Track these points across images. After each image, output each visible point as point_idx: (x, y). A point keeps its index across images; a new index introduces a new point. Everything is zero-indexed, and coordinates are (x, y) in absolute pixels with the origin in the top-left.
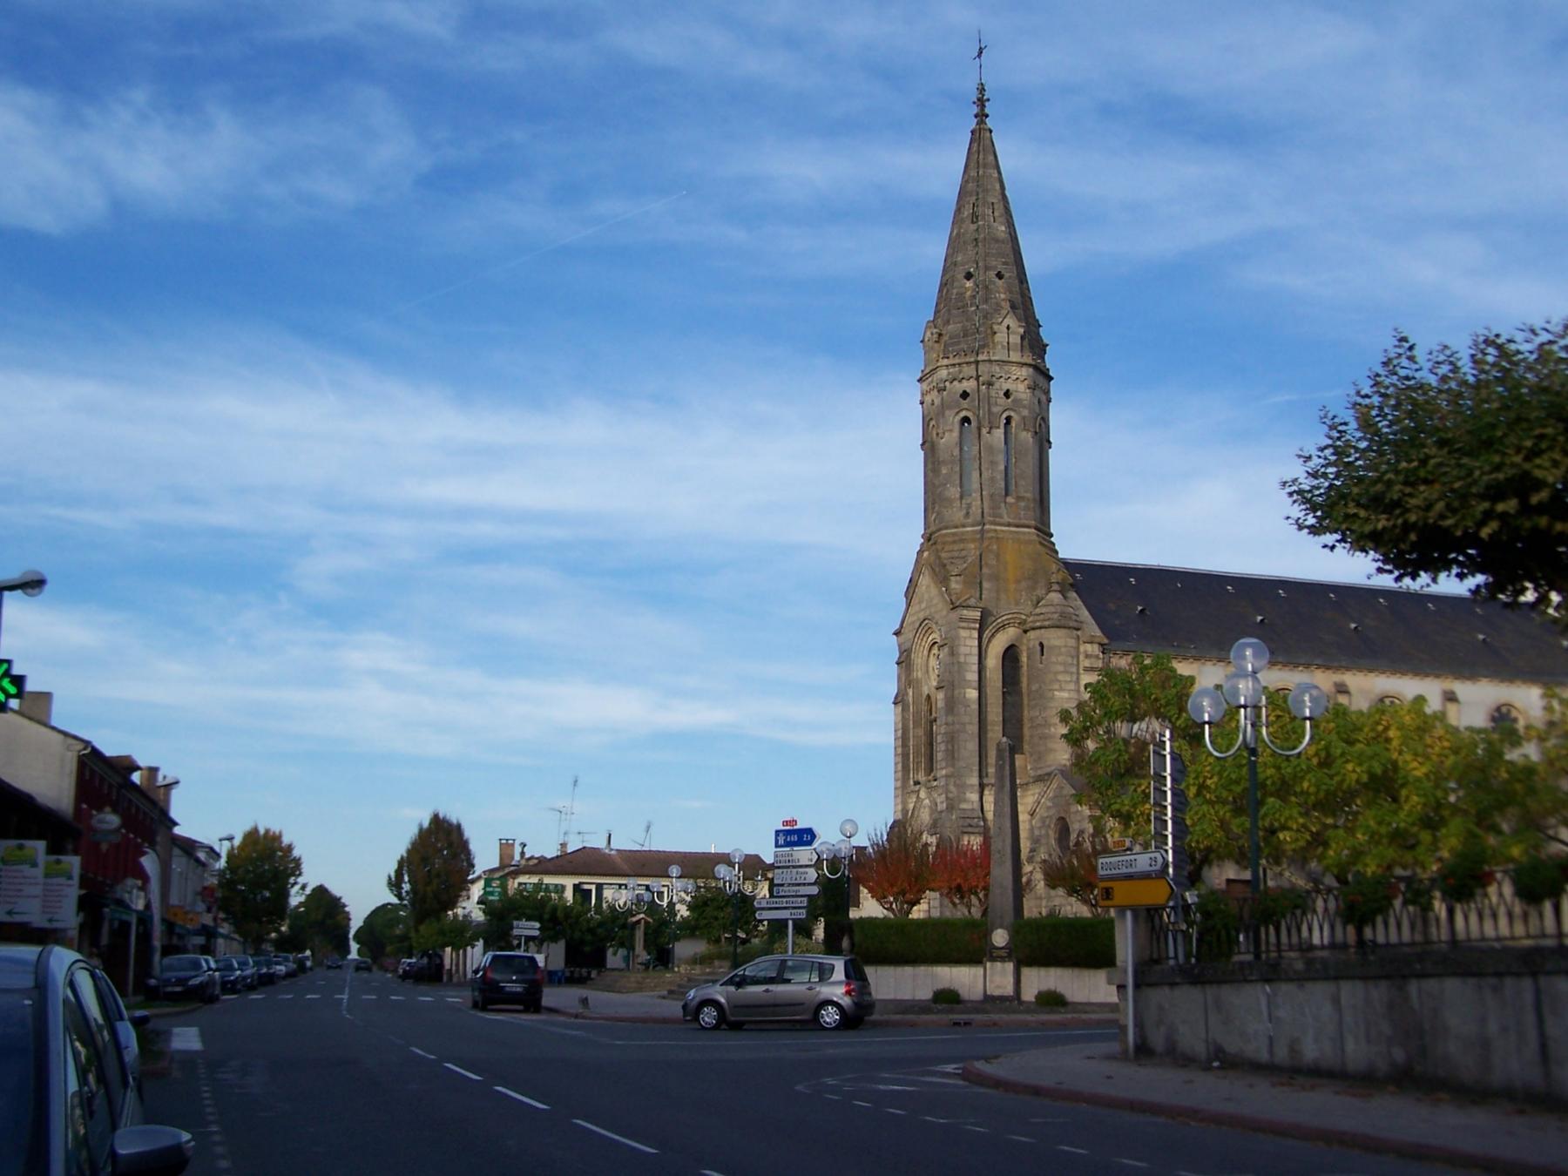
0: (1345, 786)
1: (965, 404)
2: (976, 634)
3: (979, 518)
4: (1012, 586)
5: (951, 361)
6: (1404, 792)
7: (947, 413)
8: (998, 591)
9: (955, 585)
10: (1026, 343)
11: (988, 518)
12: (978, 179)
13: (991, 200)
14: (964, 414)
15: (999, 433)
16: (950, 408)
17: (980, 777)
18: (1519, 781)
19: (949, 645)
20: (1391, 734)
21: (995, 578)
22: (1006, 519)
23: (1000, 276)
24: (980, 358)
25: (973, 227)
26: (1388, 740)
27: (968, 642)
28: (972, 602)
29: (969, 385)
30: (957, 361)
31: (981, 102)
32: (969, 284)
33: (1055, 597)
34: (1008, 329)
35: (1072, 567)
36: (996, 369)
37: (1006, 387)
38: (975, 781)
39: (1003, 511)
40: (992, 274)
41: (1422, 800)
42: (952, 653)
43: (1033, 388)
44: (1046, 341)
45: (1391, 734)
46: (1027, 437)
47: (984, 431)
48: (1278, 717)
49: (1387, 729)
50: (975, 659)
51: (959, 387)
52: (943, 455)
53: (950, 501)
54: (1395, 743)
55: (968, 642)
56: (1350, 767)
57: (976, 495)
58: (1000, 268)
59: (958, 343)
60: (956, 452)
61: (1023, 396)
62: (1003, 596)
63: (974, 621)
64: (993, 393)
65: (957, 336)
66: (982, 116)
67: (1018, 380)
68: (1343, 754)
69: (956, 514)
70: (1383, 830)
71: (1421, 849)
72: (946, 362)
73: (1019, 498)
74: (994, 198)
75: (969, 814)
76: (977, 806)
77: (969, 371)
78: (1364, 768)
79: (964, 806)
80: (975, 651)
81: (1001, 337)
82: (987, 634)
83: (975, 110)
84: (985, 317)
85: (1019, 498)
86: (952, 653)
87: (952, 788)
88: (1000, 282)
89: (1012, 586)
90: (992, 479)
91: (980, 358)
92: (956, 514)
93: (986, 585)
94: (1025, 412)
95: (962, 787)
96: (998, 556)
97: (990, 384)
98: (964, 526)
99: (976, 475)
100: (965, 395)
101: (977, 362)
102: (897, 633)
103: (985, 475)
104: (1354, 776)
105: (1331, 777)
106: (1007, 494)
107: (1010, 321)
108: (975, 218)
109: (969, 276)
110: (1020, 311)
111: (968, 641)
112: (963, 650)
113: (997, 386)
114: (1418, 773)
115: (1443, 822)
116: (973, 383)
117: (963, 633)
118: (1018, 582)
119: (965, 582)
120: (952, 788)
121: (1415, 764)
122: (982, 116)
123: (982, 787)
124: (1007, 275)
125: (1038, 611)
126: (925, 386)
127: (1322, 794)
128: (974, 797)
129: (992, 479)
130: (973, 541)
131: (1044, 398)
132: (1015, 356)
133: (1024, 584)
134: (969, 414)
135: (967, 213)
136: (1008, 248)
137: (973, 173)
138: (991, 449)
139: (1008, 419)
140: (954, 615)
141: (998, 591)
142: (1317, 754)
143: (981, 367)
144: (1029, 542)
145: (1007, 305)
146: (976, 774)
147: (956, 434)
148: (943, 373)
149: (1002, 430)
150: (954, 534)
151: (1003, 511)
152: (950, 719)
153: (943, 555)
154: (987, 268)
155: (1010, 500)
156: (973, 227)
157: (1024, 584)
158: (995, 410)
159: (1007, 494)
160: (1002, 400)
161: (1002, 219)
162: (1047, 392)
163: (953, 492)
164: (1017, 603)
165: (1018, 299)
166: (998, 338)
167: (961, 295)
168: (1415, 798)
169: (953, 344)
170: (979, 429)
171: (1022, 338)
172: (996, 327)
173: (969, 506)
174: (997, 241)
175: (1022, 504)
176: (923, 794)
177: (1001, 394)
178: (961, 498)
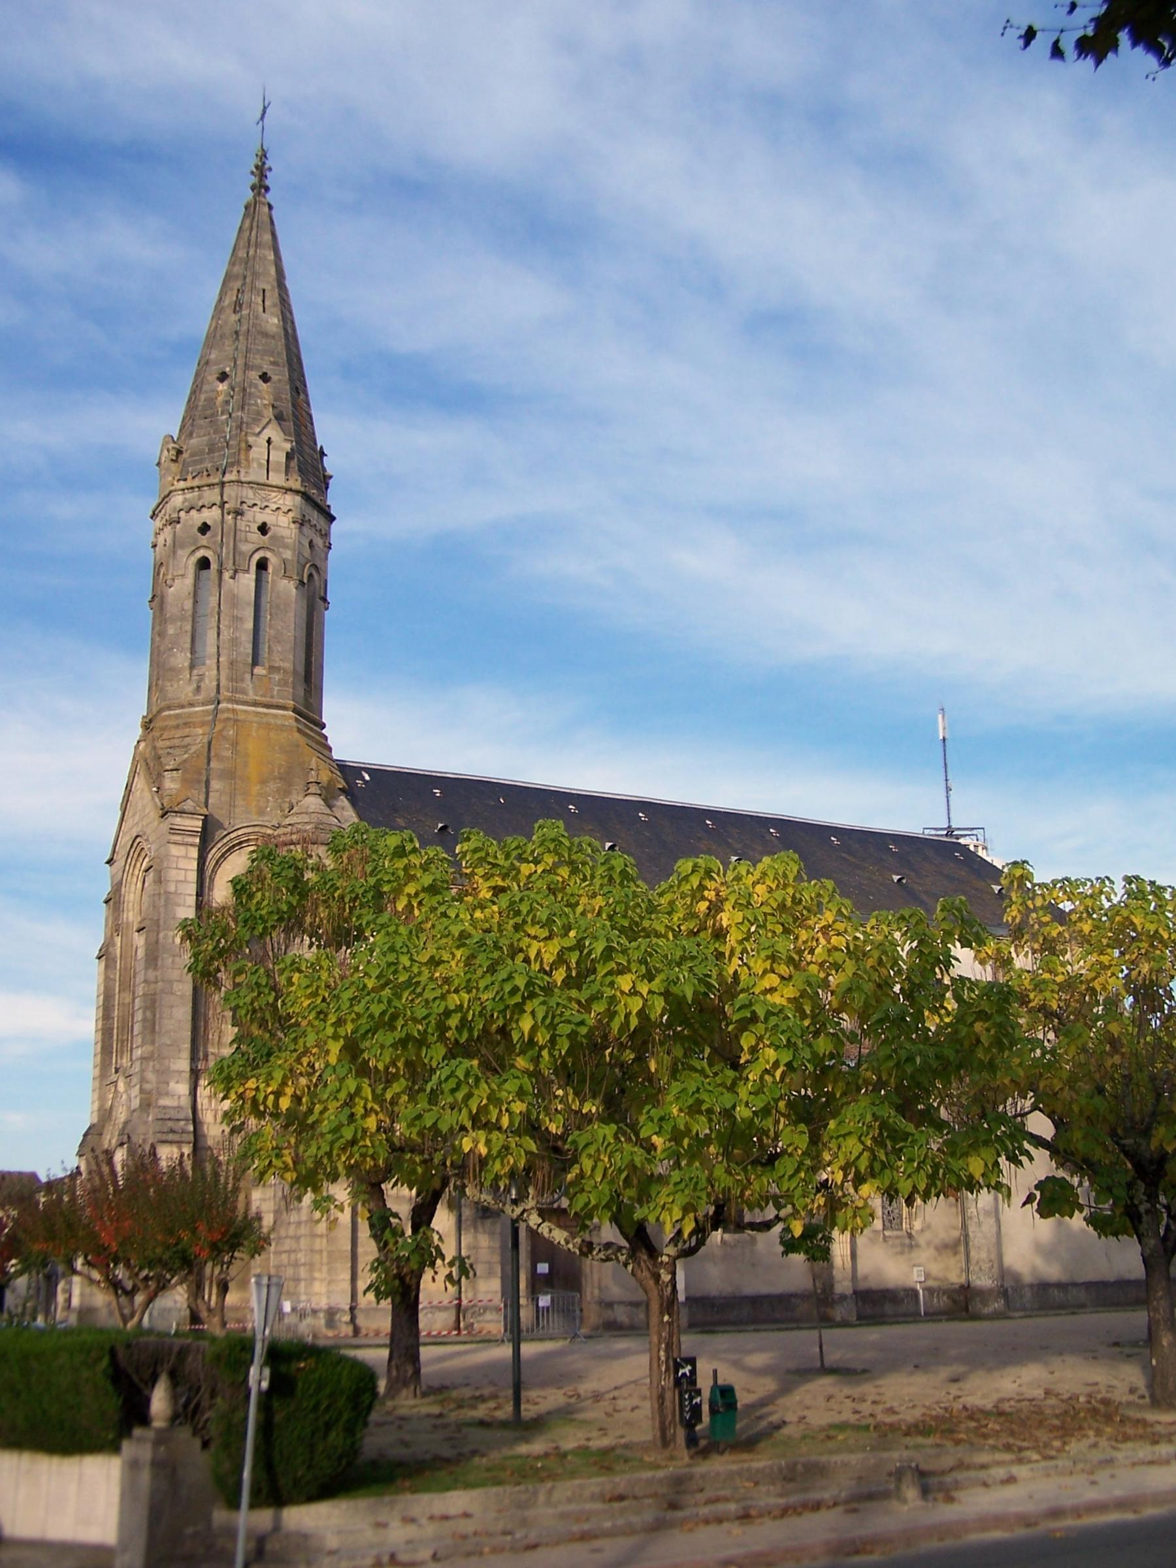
0: (1125, 1258)
1: (203, 540)
2: (194, 853)
3: (213, 694)
4: (255, 789)
5: (189, 484)
6: (747, 1041)
7: (180, 552)
8: (232, 796)
9: (171, 783)
10: (294, 464)
11: (224, 693)
12: (246, 261)
13: (261, 285)
14: (201, 553)
15: (248, 580)
16: (182, 547)
17: (194, 1058)
18: (982, 1016)
19: (157, 870)
20: (725, 919)
21: (229, 775)
22: (251, 696)
23: (265, 378)
24: (228, 477)
25: (237, 317)
26: (720, 934)
27: (182, 864)
28: (189, 806)
29: (211, 516)
30: (196, 482)
31: (261, 171)
32: (222, 387)
33: (314, 803)
34: (270, 444)
35: (344, 769)
36: (248, 494)
37: (261, 518)
38: (183, 1064)
39: (248, 684)
40: (254, 375)
41: (786, 1057)
42: (159, 881)
43: (301, 522)
44: (329, 472)
45: (725, 919)
46: (285, 588)
47: (227, 575)
48: (498, 891)
49: (716, 908)
50: (192, 889)
51: (197, 518)
52: (171, 610)
53: (175, 671)
54: (733, 938)
55: (182, 864)
56: (625, 982)
57: (211, 662)
58: (266, 368)
59: (201, 461)
60: (188, 605)
61: (286, 533)
62: (239, 801)
63: (192, 833)
64: (241, 524)
65: (202, 452)
66: (261, 188)
67: (281, 511)
68: (608, 952)
69: (182, 689)
70: (701, 1127)
71: (786, 1166)
72: (182, 484)
73: (272, 669)
74: (267, 283)
75: (172, 1114)
76: (185, 1101)
77: (213, 495)
78: (657, 985)
79: (165, 1102)
80: (193, 876)
81: (259, 452)
82: (213, 855)
83: (254, 180)
84: (240, 427)
85: (272, 669)
86: (159, 881)
87: (150, 1076)
88: (263, 386)
89: (255, 789)
90: (234, 642)
91: (228, 477)
92: (182, 689)
93: (215, 785)
94: (288, 554)
95: (164, 1074)
96: (235, 744)
97: (238, 513)
98: (191, 705)
99: (212, 635)
100: (204, 528)
101: (223, 484)
102: (110, 862)
103: (225, 635)
104: (636, 1004)
105: (586, 1007)
106: (255, 662)
107: (273, 432)
108: (238, 306)
109: (223, 377)
110: (290, 425)
111: (183, 863)
112: (173, 874)
113: (249, 515)
114: (776, 999)
115: (831, 1107)
116: (216, 512)
117: (175, 850)
118: (263, 782)
119: (184, 781)
120: (150, 1076)
121: (772, 980)
122: (261, 188)
123: (195, 1074)
124: (275, 378)
125: (287, 821)
126: (158, 523)
127: (564, 1046)
128: (181, 1088)
129: (234, 642)
130: (203, 724)
131: (319, 542)
132: (277, 478)
133: (272, 786)
134: (209, 554)
135: (230, 298)
136: (280, 345)
137: (242, 254)
138: (234, 601)
139: (262, 565)
140: (165, 826)
141: (232, 796)
142: (561, 960)
143: (227, 489)
144: (281, 728)
145: (269, 413)
146: (186, 1054)
147: (189, 580)
148: (178, 500)
149: (252, 576)
150: (177, 716)
151: (248, 684)
152: (151, 974)
153: (160, 744)
154: (247, 367)
155: (258, 670)
156: (234, 318)
157: (272, 786)
158: (245, 548)
159: (255, 662)
160: (256, 536)
161: (277, 310)
162: (326, 535)
163: (181, 659)
164: (261, 812)
165: (287, 408)
166: (253, 454)
167: (211, 401)
168: (771, 1054)
169: (195, 463)
170: (220, 573)
171: (289, 456)
172: (251, 439)
173: (201, 677)
174: (265, 335)
175: (277, 677)
176: (121, 1086)
177: (254, 527)
178: (192, 667)
